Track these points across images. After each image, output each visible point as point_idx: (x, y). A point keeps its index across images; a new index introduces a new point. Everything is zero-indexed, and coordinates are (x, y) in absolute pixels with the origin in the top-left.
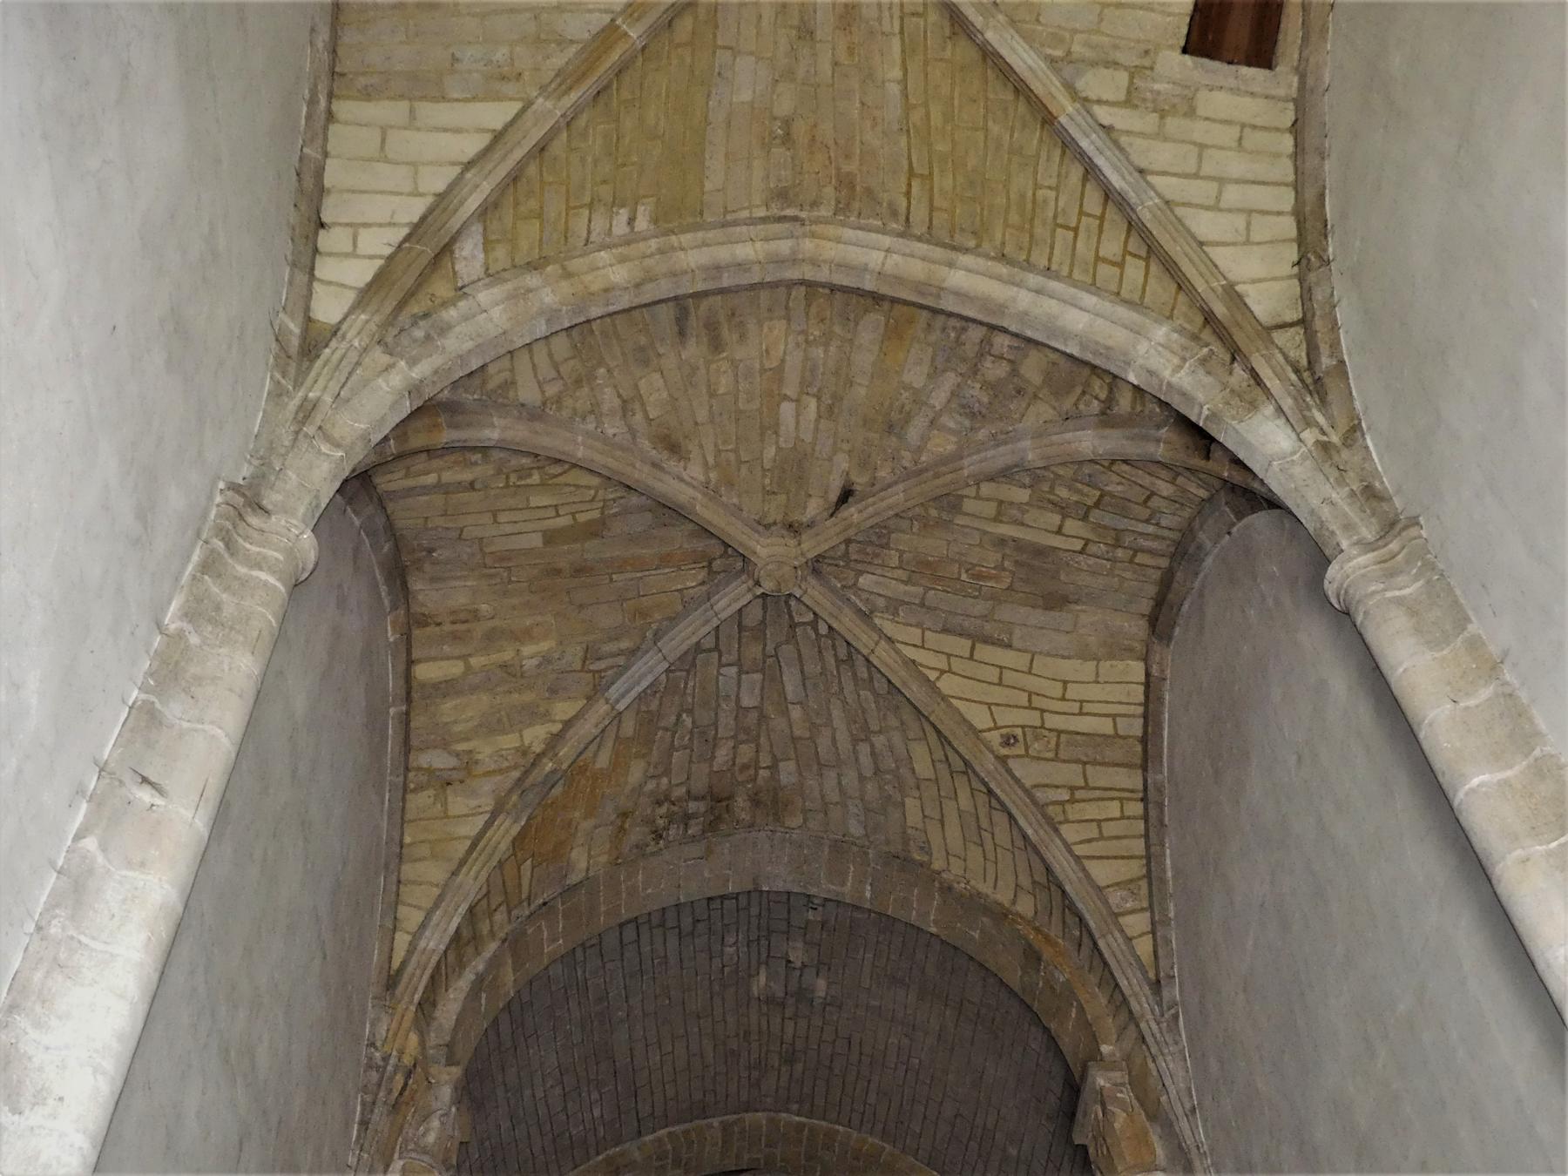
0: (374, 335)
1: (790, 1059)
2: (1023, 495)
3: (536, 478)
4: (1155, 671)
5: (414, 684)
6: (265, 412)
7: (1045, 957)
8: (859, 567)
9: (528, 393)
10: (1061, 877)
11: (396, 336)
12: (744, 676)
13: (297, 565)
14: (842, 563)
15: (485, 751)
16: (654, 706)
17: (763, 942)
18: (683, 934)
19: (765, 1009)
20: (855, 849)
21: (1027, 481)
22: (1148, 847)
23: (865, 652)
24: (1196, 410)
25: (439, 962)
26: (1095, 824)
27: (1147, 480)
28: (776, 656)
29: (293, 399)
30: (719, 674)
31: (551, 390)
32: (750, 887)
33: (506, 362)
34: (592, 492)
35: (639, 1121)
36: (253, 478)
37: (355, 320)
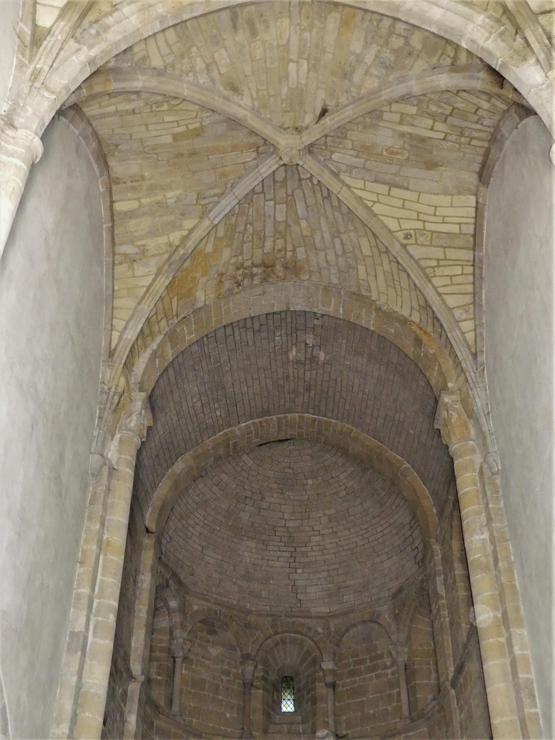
0: (69, 33)
1: (308, 389)
2: (413, 110)
3: (165, 107)
4: (480, 200)
5: (115, 212)
6: (14, 76)
7: (424, 341)
8: (332, 149)
9: (156, 62)
10: (431, 304)
11: (81, 33)
12: (277, 206)
13: (33, 156)
14: (324, 148)
15: (151, 244)
16: (233, 221)
17: (294, 335)
18: (255, 331)
19: (296, 366)
20: (334, 289)
21: (415, 102)
22: (474, 288)
23: (336, 193)
24: (495, 62)
25: (134, 344)
26: (449, 277)
27: (475, 100)
28: (293, 195)
29: (29, 69)
30: (264, 204)
31: (169, 60)
32: (285, 309)
33: (143, 44)
34: (195, 113)
35: (238, 417)
36: (9, 111)
37: (59, 25)
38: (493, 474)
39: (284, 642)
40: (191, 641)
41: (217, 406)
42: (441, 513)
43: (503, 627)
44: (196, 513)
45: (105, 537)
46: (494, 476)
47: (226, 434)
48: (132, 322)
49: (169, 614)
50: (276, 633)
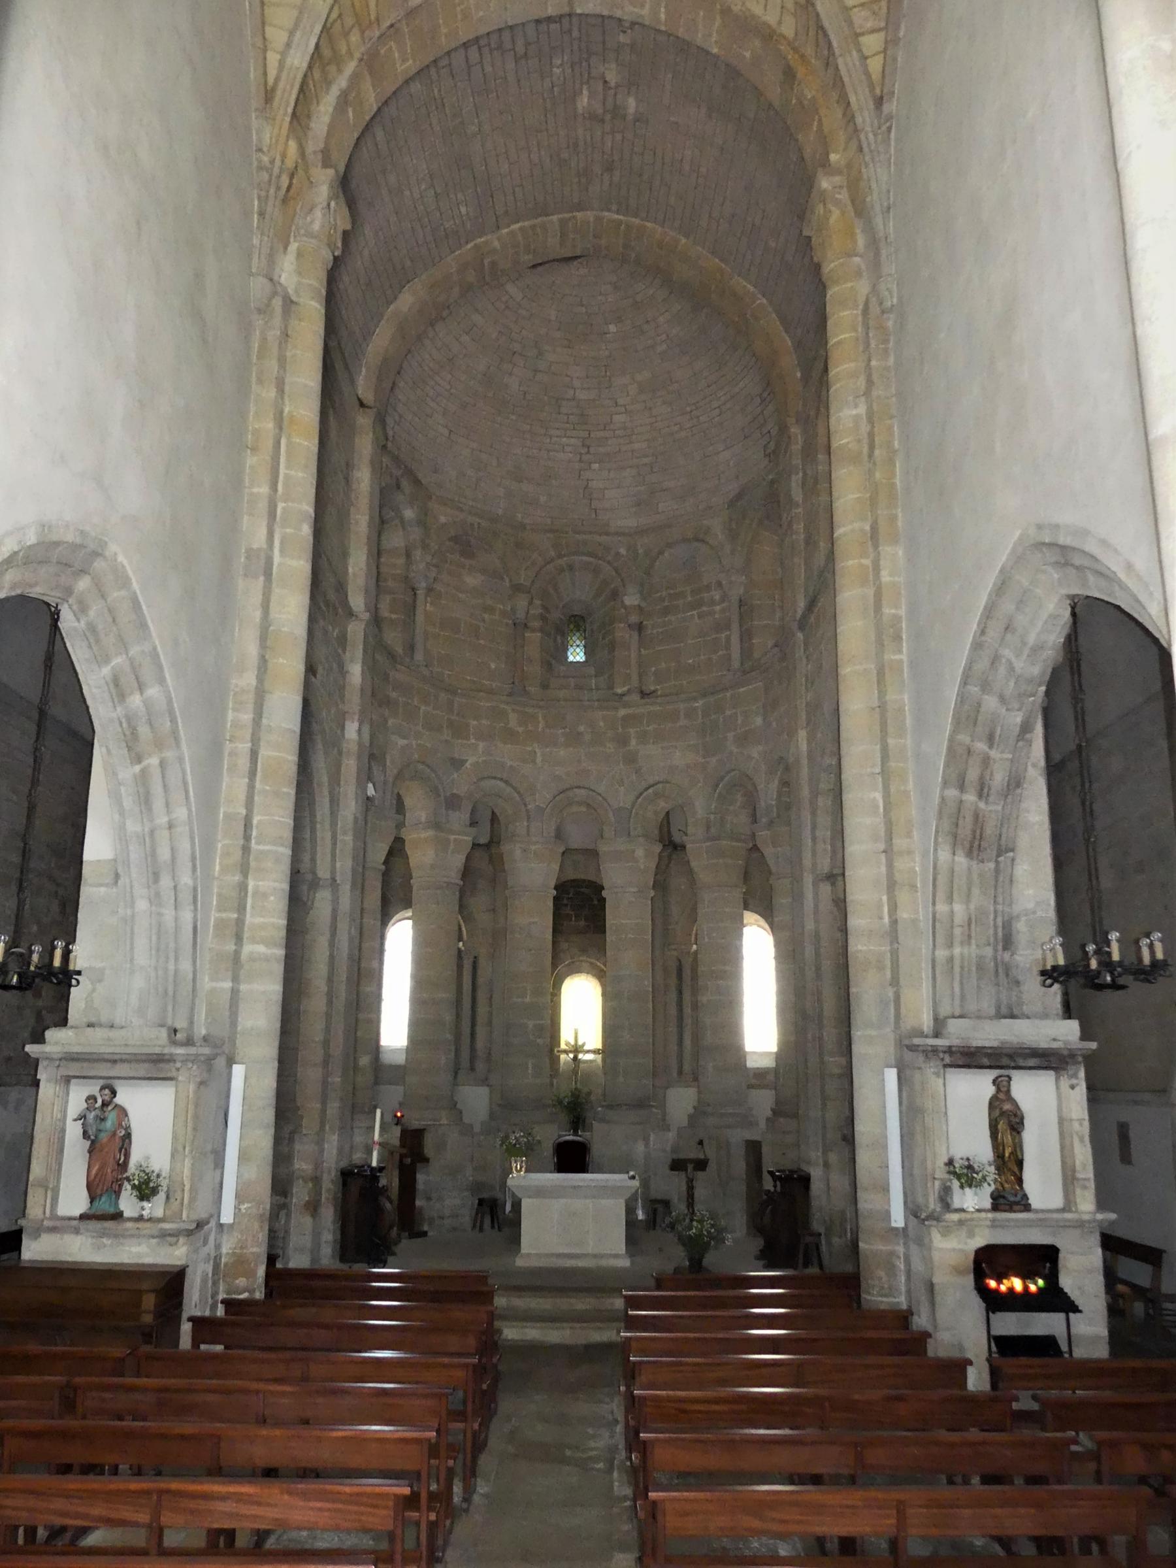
1: (609, 168)
17: (584, 64)
25: (305, 76)
32: (566, 10)
38: (883, 312)
39: (571, 568)
40: (436, 566)
41: (460, 196)
42: (806, 379)
43: (870, 543)
44: (437, 378)
45: (287, 410)
46: (885, 316)
47: (477, 247)
48: (298, 34)
49: (404, 528)
50: (560, 556)
